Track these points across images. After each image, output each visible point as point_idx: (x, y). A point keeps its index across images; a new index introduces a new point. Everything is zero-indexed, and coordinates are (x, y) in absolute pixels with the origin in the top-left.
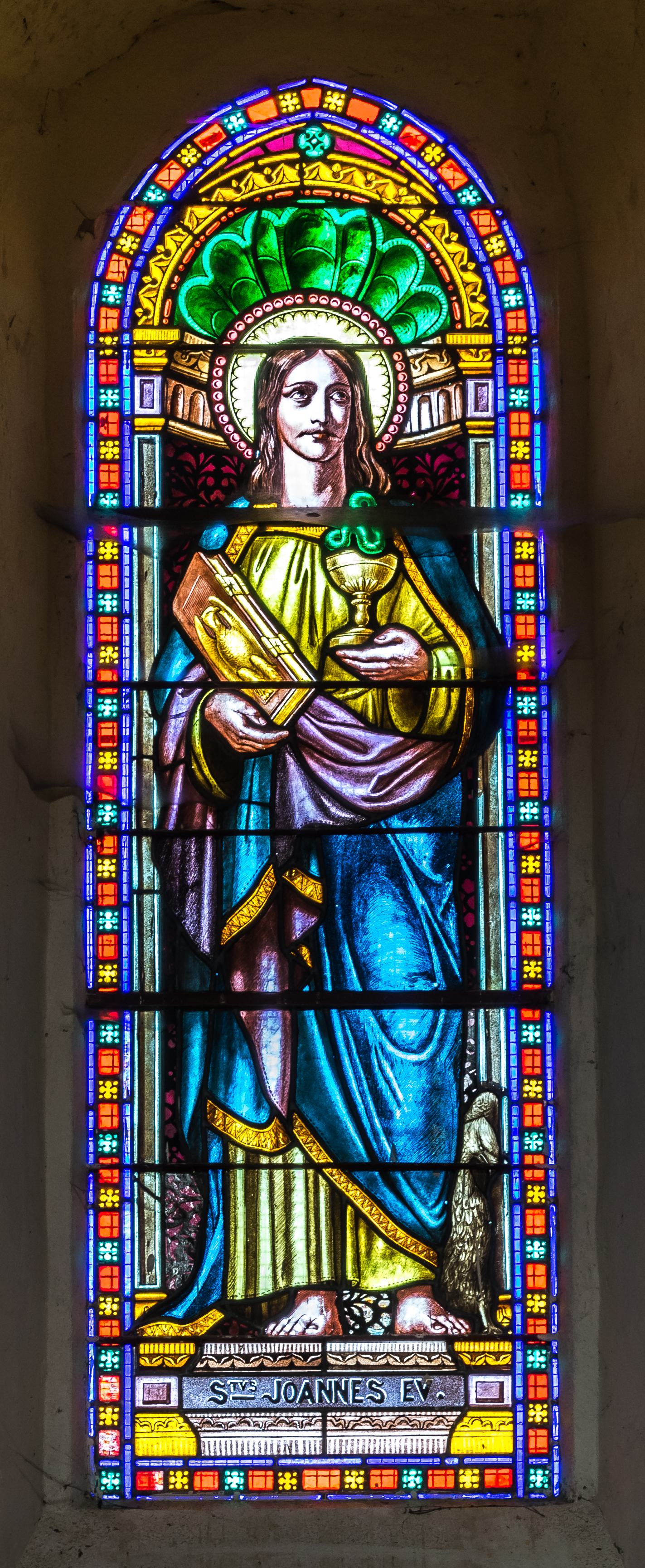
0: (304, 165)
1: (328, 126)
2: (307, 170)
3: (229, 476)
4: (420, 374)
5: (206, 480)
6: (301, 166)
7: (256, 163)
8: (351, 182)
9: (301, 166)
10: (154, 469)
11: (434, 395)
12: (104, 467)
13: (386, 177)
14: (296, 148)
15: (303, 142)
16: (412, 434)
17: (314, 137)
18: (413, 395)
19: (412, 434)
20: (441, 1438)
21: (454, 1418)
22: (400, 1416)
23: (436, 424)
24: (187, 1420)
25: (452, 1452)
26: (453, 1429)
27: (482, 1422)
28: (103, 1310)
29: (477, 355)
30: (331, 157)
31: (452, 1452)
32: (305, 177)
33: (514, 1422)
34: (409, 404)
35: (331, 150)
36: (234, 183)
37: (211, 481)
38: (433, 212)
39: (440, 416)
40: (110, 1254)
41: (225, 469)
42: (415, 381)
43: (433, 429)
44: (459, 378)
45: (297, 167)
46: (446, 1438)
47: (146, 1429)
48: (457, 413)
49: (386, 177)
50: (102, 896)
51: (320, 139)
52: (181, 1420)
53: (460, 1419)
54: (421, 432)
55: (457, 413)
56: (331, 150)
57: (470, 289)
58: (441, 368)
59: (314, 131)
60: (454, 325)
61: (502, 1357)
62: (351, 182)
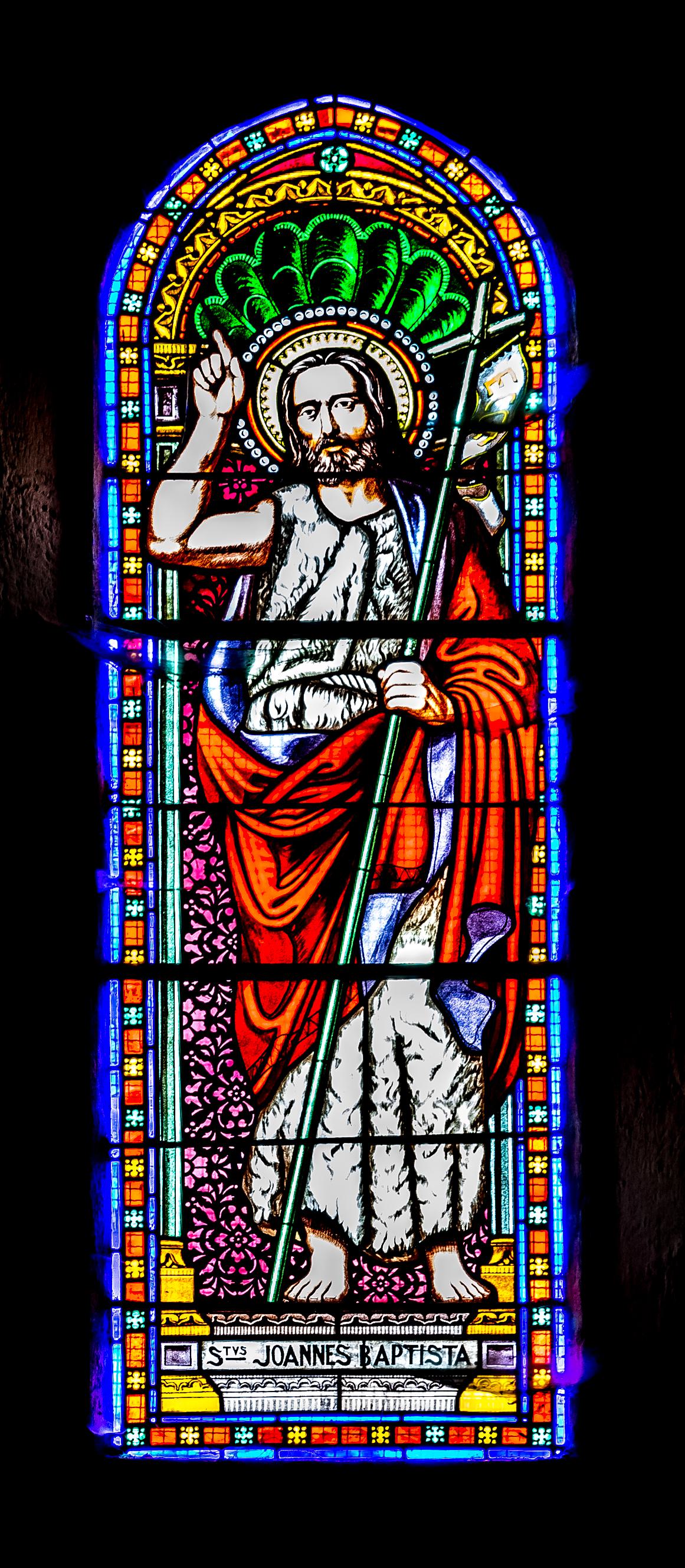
8: (461, 247)
13: (472, 233)
20: (449, 1399)
22: (407, 1378)
24: (210, 1382)
25: (462, 1409)
28: (130, 912)
31: (462, 1409)
38: (213, 225)
40: (135, 707)
45: (455, 226)
46: (454, 1398)
47: (171, 1389)
49: (472, 233)
50: (129, 371)
51: (332, 164)
52: (204, 1381)
57: (208, 241)
61: (505, 1320)
62: (461, 247)
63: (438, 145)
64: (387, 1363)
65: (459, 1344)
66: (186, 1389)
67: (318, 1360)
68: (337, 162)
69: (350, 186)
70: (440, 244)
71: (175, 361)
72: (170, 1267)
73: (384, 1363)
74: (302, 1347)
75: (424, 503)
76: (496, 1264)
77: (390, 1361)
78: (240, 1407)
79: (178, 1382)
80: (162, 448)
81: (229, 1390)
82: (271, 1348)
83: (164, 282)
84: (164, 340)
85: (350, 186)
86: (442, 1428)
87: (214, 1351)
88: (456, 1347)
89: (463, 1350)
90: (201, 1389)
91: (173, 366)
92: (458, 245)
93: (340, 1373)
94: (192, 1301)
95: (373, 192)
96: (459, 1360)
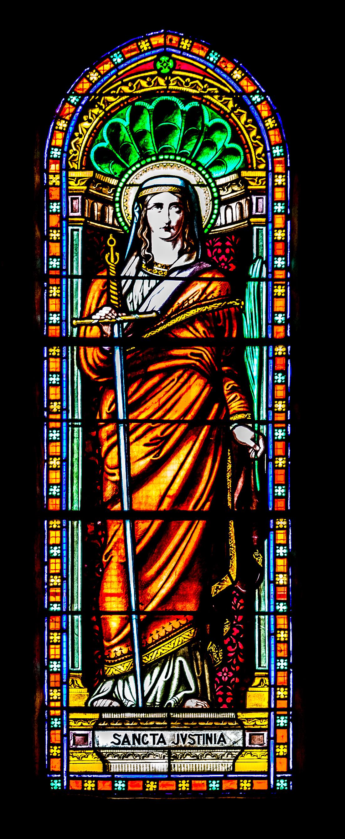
0: (99, 103)
1: (174, 56)
2: (171, 81)
3: (229, 247)
4: (227, 193)
5: (217, 250)
6: (98, 104)
7: (122, 82)
9: (168, 78)
10: (263, 240)
11: (233, 205)
12: (58, 657)
14: (155, 69)
15: (159, 65)
16: (221, 226)
17: (165, 62)
18: (221, 206)
19: (221, 226)
21: (237, 754)
22: (206, 752)
23: (235, 220)
26: (236, 758)
27: (251, 754)
29: (258, 183)
30: (174, 72)
32: (104, 108)
33: (269, 755)
34: (219, 210)
35: (174, 69)
36: (130, 85)
37: (220, 251)
39: (237, 217)
41: (228, 243)
42: (223, 198)
43: (233, 223)
44: (247, 194)
47: (75, 759)
48: (246, 214)
51: (161, 66)
53: (240, 753)
54: (226, 225)
55: (246, 214)
56: (174, 69)
58: (238, 190)
59: (164, 59)
60: (247, 166)
63: (101, 62)
64: (129, 744)
65: (159, 733)
66: (84, 759)
67: (136, 742)
68: (165, 62)
69: (139, 82)
70: (225, 115)
71: (261, 181)
72: (264, 687)
73: (163, 744)
74: (134, 736)
75: (106, 262)
76: (256, 687)
77: (131, 743)
78: (134, 770)
79: (79, 754)
80: (72, 230)
81: (148, 758)
82: (141, 736)
83: (73, 137)
84: (74, 170)
85: (139, 82)
86: (124, 782)
87: (116, 736)
88: (157, 734)
89: (162, 736)
90: (93, 759)
91: (260, 183)
92: (96, 118)
93: (169, 749)
94: (286, 707)
95: (134, 86)
96: (159, 742)
